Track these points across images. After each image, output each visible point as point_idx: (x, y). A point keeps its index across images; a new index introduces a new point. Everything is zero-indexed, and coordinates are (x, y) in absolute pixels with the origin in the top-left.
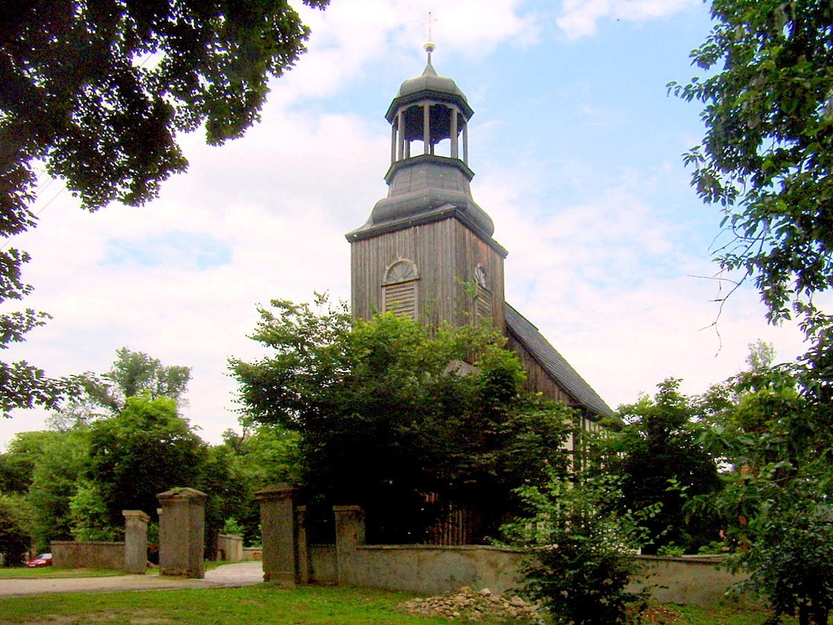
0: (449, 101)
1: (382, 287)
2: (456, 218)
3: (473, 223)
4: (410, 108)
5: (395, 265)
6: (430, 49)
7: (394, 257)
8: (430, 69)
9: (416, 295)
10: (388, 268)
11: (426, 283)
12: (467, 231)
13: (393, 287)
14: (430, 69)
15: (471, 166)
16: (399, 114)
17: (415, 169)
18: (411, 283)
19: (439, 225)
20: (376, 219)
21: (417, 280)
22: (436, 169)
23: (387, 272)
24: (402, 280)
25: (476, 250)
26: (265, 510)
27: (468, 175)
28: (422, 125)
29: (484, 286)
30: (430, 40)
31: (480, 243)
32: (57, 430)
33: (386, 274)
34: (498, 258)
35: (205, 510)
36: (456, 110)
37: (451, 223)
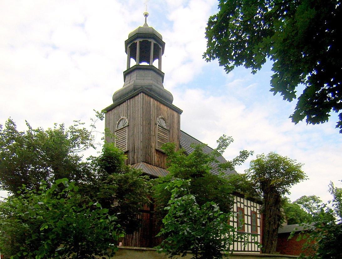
0: (149, 38)
1: (115, 132)
2: (143, 93)
3: (165, 99)
4: (131, 45)
5: (120, 121)
6: (146, 15)
7: (120, 117)
8: (146, 24)
9: (127, 134)
10: (117, 123)
11: (131, 126)
12: (152, 100)
13: (120, 131)
14: (146, 24)
15: (163, 70)
16: (138, 41)
17: (132, 74)
18: (125, 128)
19: (137, 97)
20: (114, 100)
21: (127, 126)
22: (142, 72)
23: (117, 124)
24: (123, 127)
25: (158, 109)
26: (27, 243)
27: (162, 75)
28: (136, 49)
29: (165, 127)
30: (146, 11)
31: (162, 106)
32: (308, 213)
33: (117, 125)
34: (176, 114)
35: (278, 231)
36: (153, 42)
37: (141, 95)
